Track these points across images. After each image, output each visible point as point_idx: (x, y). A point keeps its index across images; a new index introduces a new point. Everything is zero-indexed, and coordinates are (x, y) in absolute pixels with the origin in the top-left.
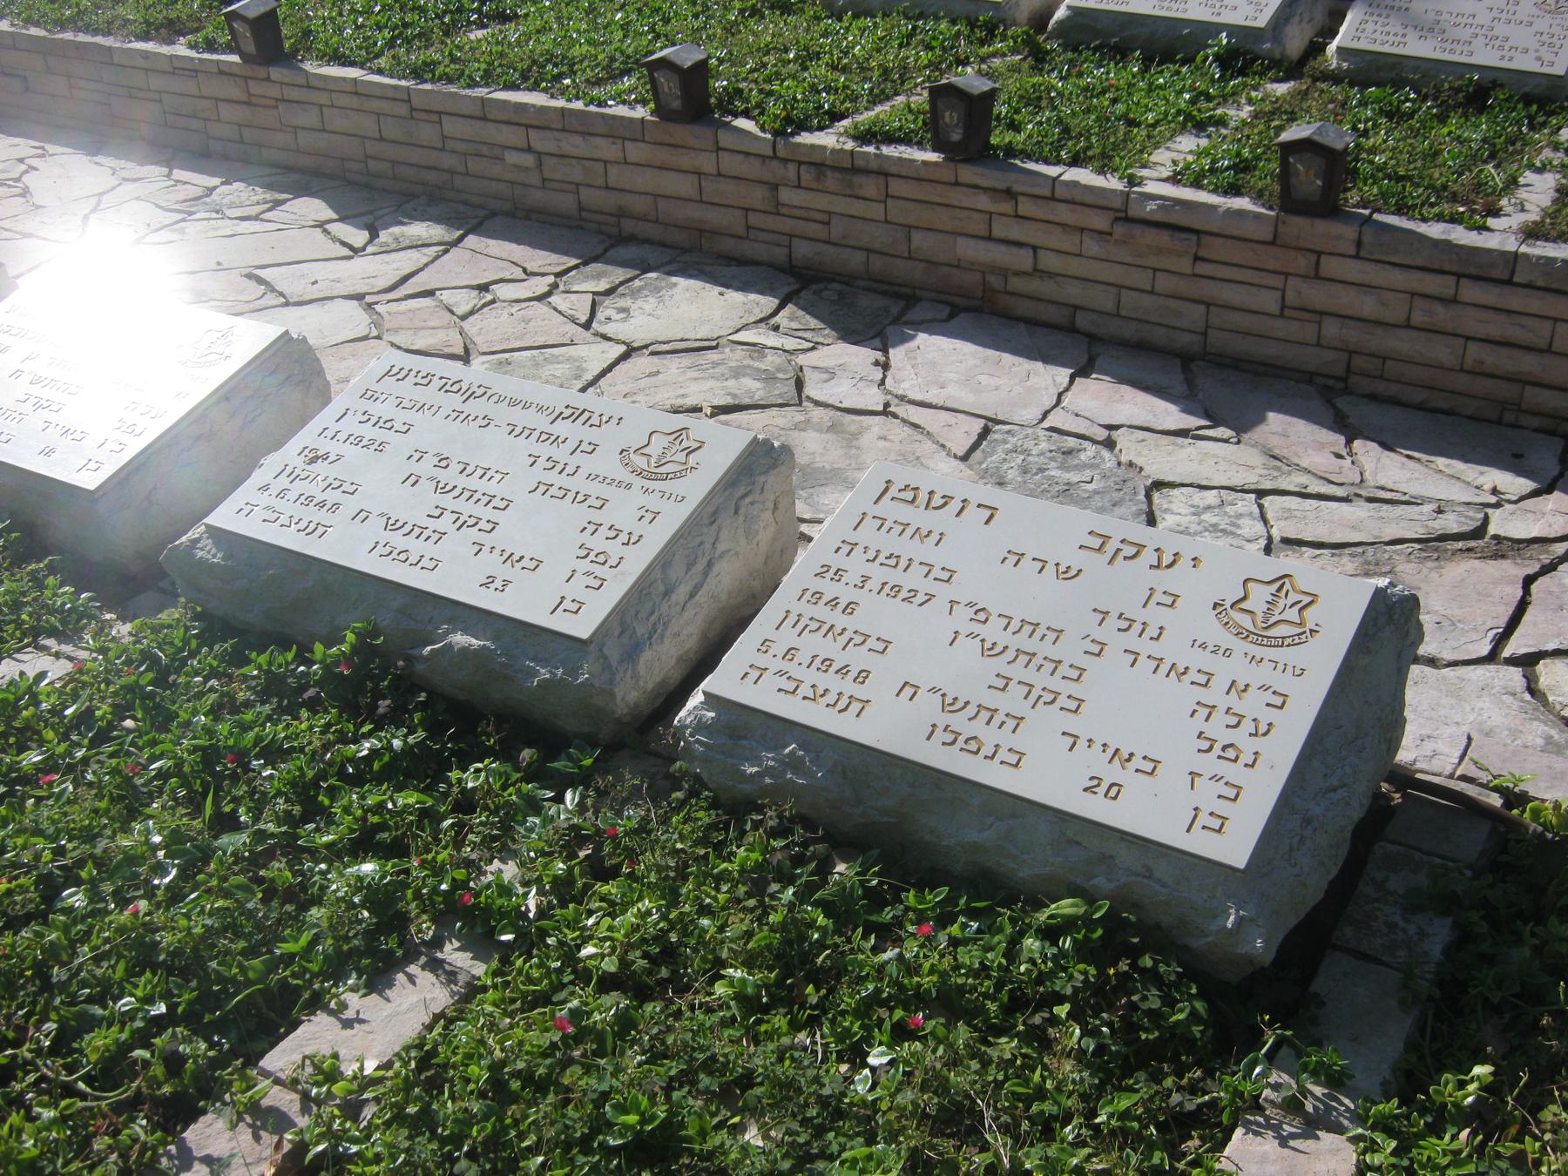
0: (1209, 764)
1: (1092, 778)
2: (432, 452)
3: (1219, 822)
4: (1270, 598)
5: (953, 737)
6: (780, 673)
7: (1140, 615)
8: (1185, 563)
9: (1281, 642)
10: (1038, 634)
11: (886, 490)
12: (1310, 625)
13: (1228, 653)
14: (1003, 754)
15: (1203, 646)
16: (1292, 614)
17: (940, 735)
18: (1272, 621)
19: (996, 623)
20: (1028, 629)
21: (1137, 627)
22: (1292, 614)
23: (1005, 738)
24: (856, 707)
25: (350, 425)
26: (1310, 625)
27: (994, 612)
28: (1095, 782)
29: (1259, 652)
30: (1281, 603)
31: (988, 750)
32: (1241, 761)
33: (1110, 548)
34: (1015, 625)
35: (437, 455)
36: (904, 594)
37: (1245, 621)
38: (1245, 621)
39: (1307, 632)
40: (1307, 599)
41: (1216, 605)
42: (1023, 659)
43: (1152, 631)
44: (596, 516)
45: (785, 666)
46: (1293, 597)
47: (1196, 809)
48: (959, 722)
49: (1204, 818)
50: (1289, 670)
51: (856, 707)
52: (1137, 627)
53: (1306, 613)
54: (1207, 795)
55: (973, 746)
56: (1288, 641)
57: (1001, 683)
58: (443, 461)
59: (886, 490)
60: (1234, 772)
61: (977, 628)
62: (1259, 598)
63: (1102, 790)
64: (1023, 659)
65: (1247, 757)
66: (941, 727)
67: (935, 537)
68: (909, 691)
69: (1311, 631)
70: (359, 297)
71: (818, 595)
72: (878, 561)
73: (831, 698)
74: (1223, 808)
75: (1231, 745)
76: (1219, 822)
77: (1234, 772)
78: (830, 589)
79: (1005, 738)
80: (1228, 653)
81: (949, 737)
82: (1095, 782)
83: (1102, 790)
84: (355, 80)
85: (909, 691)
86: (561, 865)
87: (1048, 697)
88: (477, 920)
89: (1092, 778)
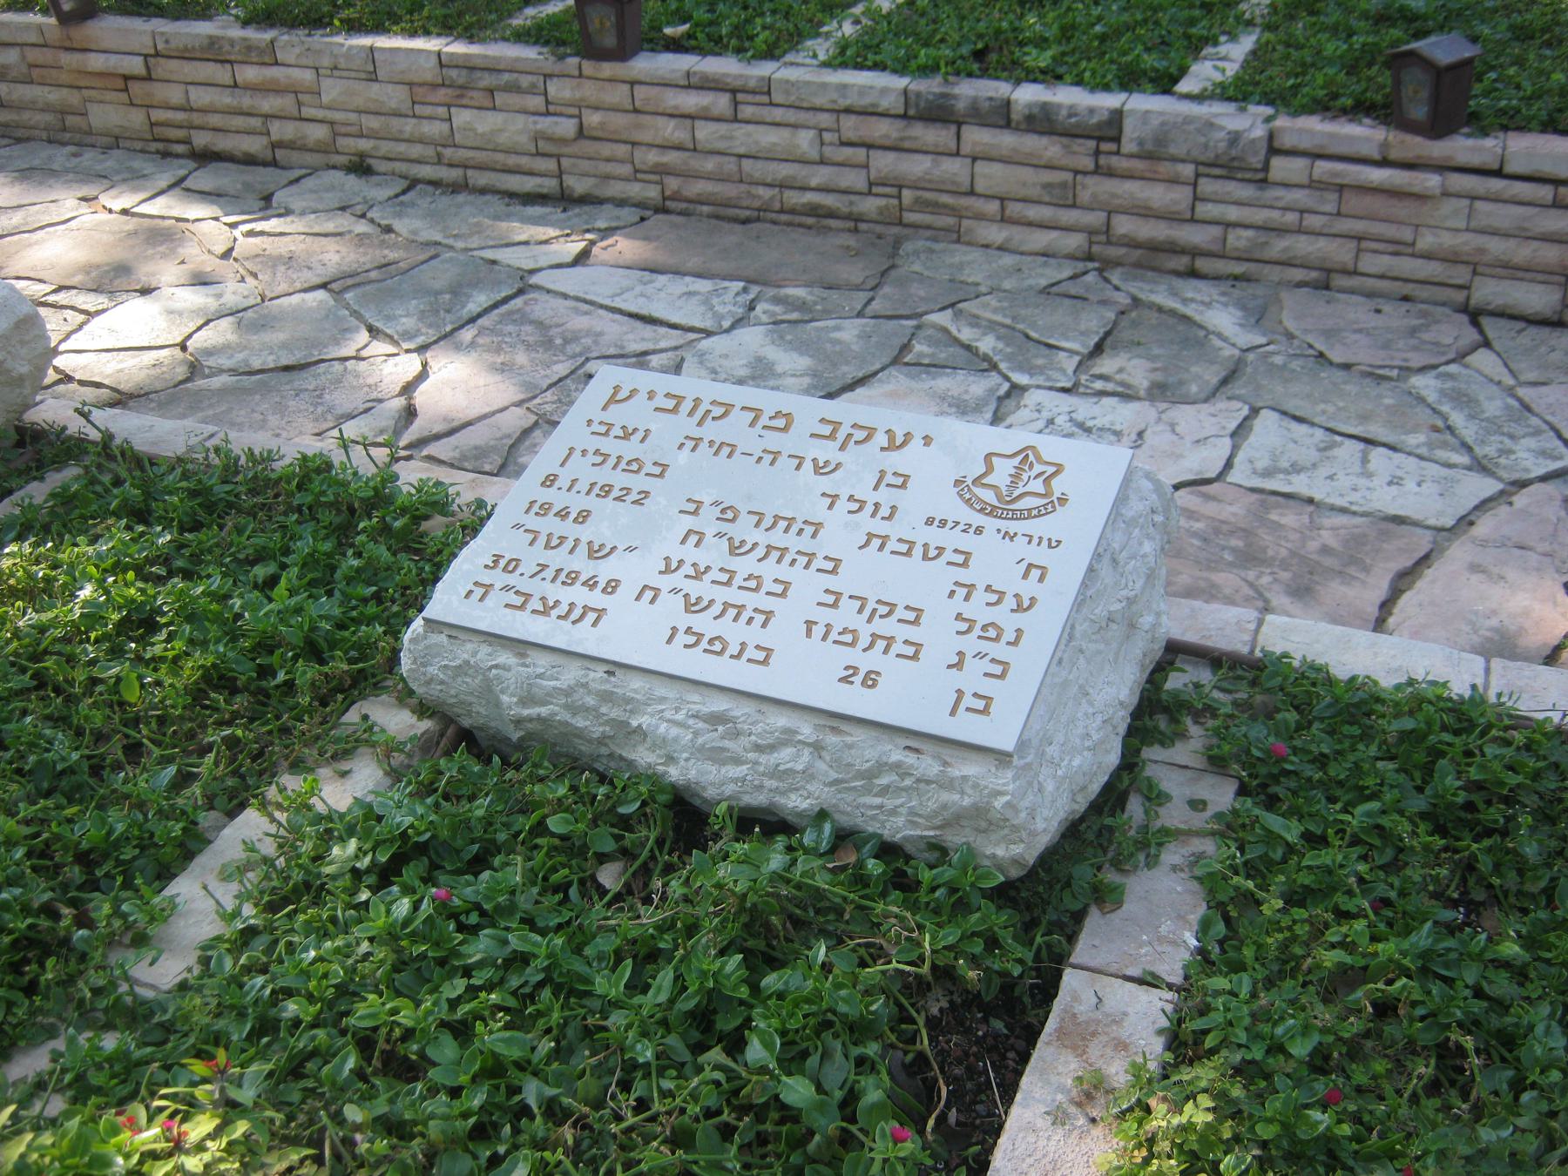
0: (971, 644)
2: (707, 500)
6: (507, 588)
8: (917, 442)
9: (1028, 515)
10: (795, 529)
13: (979, 531)
14: (751, 653)
15: (943, 523)
17: (682, 639)
19: (746, 521)
20: (782, 524)
23: (754, 635)
24: (592, 616)
25: (582, 469)
26: (1057, 494)
27: (743, 508)
29: (1013, 526)
30: (1025, 477)
31: (734, 649)
32: (1004, 639)
33: (841, 435)
34: (768, 522)
35: (716, 504)
36: (616, 493)
37: (989, 496)
39: (1053, 503)
40: (1051, 470)
42: (775, 555)
43: (884, 511)
44: (964, 576)
45: (511, 579)
46: (1038, 468)
48: (704, 623)
49: (968, 701)
50: (1045, 543)
51: (592, 616)
52: (869, 508)
53: (1054, 482)
54: (972, 678)
55: (717, 647)
57: (831, 599)
58: (728, 514)
60: (1000, 650)
61: (724, 527)
62: (1002, 474)
63: (858, 679)
64: (775, 555)
65: (1009, 636)
66: (682, 629)
67: (640, 435)
68: (649, 594)
70: (324, 286)
71: (545, 508)
73: (563, 609)
74: (989, 687)
75: (992, 624)
77: (1000, 650)
78: (557, 497)
79: (754, 635)
80: (979, 531)
81: (692, 639)
83: (858, 679)
85: (649, 594)
86: (649, 1054)
87: (883, 610)
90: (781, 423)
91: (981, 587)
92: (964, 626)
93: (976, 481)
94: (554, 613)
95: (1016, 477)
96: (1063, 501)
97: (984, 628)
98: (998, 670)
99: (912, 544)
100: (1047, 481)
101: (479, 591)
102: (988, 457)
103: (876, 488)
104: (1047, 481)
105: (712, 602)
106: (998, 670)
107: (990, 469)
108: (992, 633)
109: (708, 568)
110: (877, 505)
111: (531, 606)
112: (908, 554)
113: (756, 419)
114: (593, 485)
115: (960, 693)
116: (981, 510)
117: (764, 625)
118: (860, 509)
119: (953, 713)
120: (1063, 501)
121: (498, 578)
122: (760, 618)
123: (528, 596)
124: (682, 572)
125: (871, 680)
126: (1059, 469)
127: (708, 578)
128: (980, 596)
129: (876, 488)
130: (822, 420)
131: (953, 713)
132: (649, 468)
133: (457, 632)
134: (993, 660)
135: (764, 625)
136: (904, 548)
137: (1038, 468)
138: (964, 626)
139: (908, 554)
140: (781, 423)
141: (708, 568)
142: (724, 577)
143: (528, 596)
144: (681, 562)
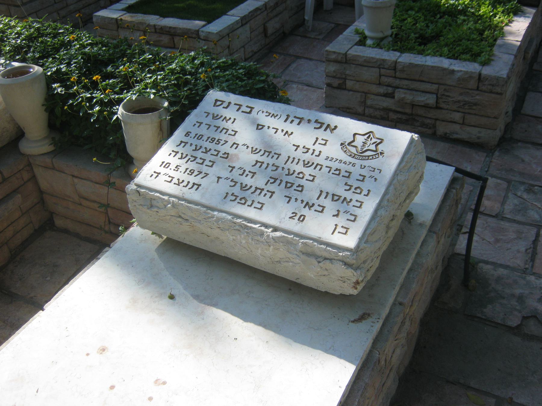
1: (293, 213)
3: (321, 208)
4: (364, 141)
5: (235, 198)
7: (312, 148)
11: (336, 228)
12: (380, 151)
13: (354, 165)
16: (373, 147)
18: (364, 150)
21: (311, 151)
22: (373, 147)
26: (380, 151)
28: (294, 215)
30: (368, 143)
37: (353, 150)
38: (353, 150)
39: (379, 154)
40: (379, 141)
41: (342, 144)
43: (317, 153)
46: (374, 140)
47: (336, 225)
51: (196, 187)
53: (379, 146)
56: (371, 157)
59: (336, 228)
62: (360, 140)
66: (230, 193)
67: (232, 120)
69: (381, 153)
72: (253, 206)
73: (185, 184)
76: (321, 208)
82: (294, 215)
83: (297, 218)
84: (116, 19)
88: (155, 57)
89: (293, 213)
91: (301, 147)
93: (349, 144)
94: (182, 185)
96: (381, 153)
98: (352, 218)
100: (377, 145)
101: (155, 175)
102: (355, 135)
103: (314, 145)
104: (377, 145)
105: (251, 187)
109: (210, 150)
110: (314, 150)
114: (209, 138)
116: (350, 156)
117: (271, 197)
118: (307, 152)
121: (162, 170)
122: (269, 194)
124: (201, 150)
125: (302, 219)
126: (382, 141)
127: (209, 153)
128: (300, 149)
129: (314, 145)
130: (360, 175)
132: (230, 132)
134: (351, 214)
135: (271, 197)
141: (210, 150)
142: (216, 153)
144: (201, 147)
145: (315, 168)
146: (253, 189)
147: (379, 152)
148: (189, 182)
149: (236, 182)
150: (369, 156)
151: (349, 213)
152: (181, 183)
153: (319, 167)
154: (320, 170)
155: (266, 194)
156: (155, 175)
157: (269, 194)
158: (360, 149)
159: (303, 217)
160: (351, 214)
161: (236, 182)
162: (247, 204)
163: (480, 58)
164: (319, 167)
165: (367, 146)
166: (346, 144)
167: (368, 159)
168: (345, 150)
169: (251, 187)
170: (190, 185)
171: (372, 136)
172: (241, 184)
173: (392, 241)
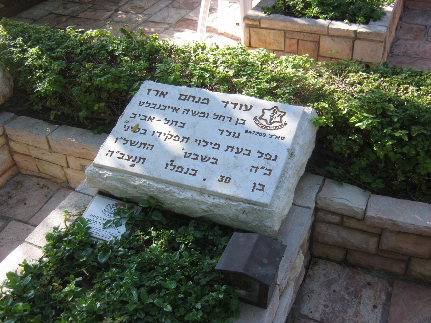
4: (271, 114)
9: (276, 128)
12: (284, 122)
14: (191, 172)
18: (272, 121)
22: (278, 119)
26: (284, 122)
30: (274, 116)
31: (185, 170)
37: (264, 123)
40: (282, 114)
46: (278, 113)
51: (142, 161)
90: (206, 101)
92: (260, 155)
93: (260, 118)
94: (131, 160)
95: (272, 116)
97: (266, 155)
99: (198, 156)
101: (110, 153)
105: (138, 142)
106: (268, 172)
107: (263, 115)
108: (268, 157)
111: (124, 158)
112: (196, 159)
113: (158, 93)
115: (255, 184)
116: (262, 127)
119: (253, 191)
120: (286, 124)
123: (124, 155)
131: (253, 191)
133: (101, 167)
134: (267, 169)
136: (195, 157)
137: (278, 113)
138: (260, 155)
139: (196, 159)
140: (206, 101)
143: (124, 155)
145: (219, 119)
146: (139, 144)
147: (283, 123)
148: (136, 157)
149: (127, 141)
150: (276, 127)
151: (265, 168)
152: (131, 158)
153: (222, 118)
154: (223, 120)
155: (148, 147)
156: (110, 153)
157: (150, 147)
158: (268, 121)
159: (228, 179)
160: (267, 169)
161: (127, 141)
162: (183, 172)
163: (284, 184)
164: (222, 118)
165: (273, 119)
166: (258, 118)
167: (276, 129)
168: (257, 123)
169: (138, 142)
170: (138, 160)
171: (276, 110)
172: (131, 141)
173: (374, 217)
